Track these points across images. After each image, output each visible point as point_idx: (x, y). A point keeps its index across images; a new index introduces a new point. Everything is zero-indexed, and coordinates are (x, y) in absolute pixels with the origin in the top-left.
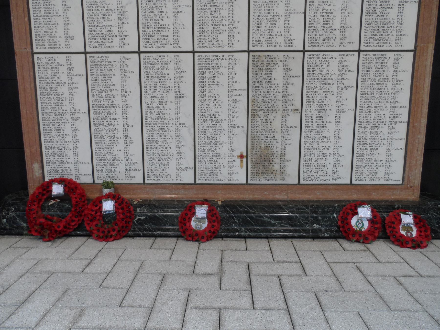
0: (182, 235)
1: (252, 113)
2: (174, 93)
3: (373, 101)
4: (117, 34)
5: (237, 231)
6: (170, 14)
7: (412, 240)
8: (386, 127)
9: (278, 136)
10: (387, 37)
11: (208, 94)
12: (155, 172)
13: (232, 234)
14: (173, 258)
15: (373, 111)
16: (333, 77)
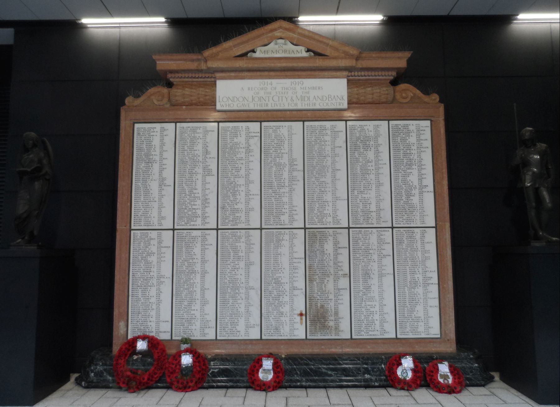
0: (251, 385)
1: (309, 279)
2: (244, 262)
3: (407, 267)
4: (200, 215)
5: (298, 381)
6: (243, 200)
7: (448, 386)
8: (421, 288)
9: (331, 296)
10: (413, 217)
11: (272, 262)
12: (226, 329)
13: (294, 384)
14: (246, 403)
15: (408, 275)
16: (374, 248)
